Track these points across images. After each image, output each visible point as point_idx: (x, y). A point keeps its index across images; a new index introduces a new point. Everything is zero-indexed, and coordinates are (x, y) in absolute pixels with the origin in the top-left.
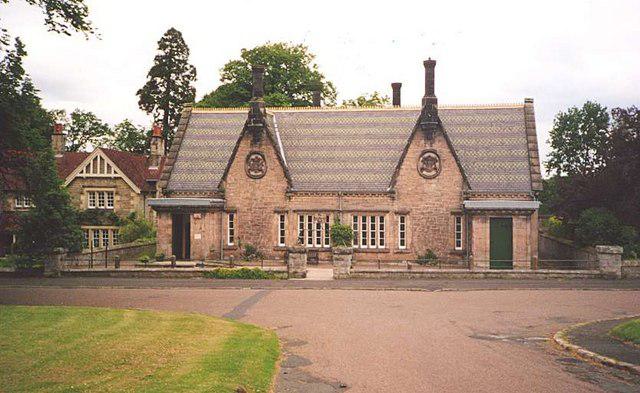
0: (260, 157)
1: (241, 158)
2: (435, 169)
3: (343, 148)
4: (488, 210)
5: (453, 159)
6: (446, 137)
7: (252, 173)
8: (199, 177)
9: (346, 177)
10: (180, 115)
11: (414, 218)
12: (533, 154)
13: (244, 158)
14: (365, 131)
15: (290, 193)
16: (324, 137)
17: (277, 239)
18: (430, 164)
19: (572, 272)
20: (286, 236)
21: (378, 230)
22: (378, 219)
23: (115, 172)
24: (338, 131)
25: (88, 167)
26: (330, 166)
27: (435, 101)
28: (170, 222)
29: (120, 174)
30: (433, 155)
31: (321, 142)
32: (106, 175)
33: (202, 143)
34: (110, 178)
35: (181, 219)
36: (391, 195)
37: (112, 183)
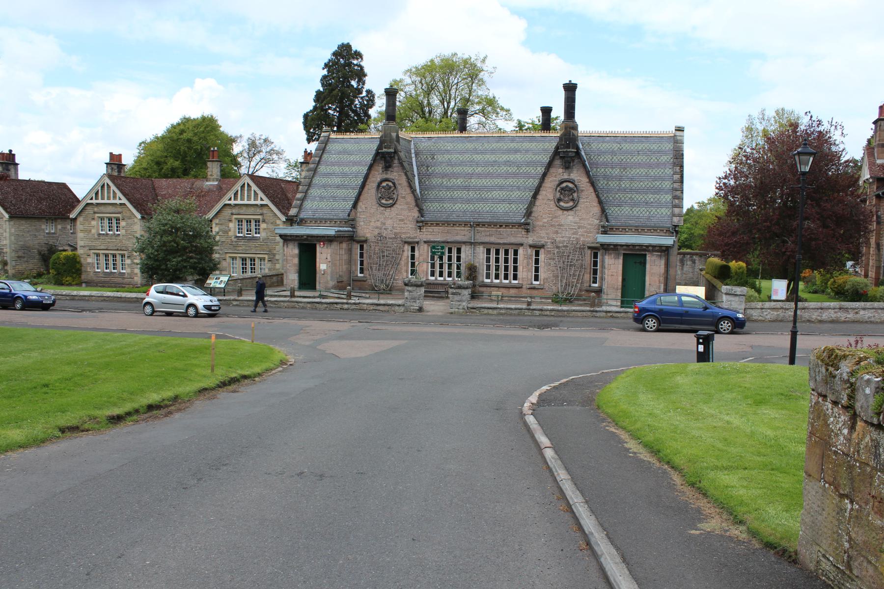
0: (390, 184)
1: (372, 186)
2: (573, 200)
3: (480, 176)
4: (622, 246)
5: (591, 190)
6: (584, 166)
7: (383, 201)
8: (458, 206)
9: (479, 206)
11: (549, 252)
12: (676, 185)
13: (375, 185)
14: (505, 157)
15: (421, 224)
16: (462, 164)
17: (407, 272)
18: (567, 194)
20: (417, 268)
21: (511, 264)
22: (511, 252)
23: (262, 199)
24: (478, 157)
25: (236, 194)
27: (575, 128)
28: (296, 251)
29: (266, 201)
30: (571, 185)
31: (457, 169)
32: (252, 202)
34: (257, 205)
35: (308, 249)
36: (526, 227)
37: (259, 211)
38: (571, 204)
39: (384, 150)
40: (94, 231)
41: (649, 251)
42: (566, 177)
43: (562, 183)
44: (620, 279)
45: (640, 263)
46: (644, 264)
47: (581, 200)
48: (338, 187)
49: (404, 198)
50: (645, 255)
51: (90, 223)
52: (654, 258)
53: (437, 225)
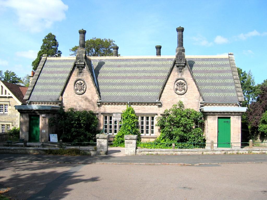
3: (130, 78)
5: (194, 83)
10: (12, 79)
13: (73, 83)
14: (142, 69)
26: (123, 87)
29: (12, 95)
30: (182, 81)
32: (4, 95)
33: (51, 75)
38: (183, 91)
42: (180, 77)
48: (52, 84)
49: (90, 89)
53: (109, 104)
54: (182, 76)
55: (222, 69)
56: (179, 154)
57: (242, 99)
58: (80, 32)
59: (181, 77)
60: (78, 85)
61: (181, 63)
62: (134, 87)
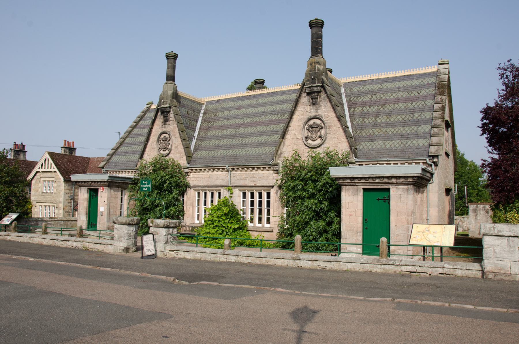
2: (320, 137)
14: (272, 108)
19: (14, 257)
22: (265, 195)
29: (56, 169)
30: (318, 122)
32: (49, 170)
34: (51, 172)
39: (163, 106)
40: (40, 190)
41: (392, 184)
42: (313, 114)
43: (310, 119)
44: (360, 219)
45: (385, 200)
46: (388, 200)
47: (329, 137)
50: (389, 190)
51: (38, 185)
52: (400, 192)
54: (317, 112)
55: (417, 94)
56: (233, 261)
57: (437, 151)
58: (168, 57)
59: (316, 114)
60: (162, 141)
61: (317, 85)
62: (246, 141)
